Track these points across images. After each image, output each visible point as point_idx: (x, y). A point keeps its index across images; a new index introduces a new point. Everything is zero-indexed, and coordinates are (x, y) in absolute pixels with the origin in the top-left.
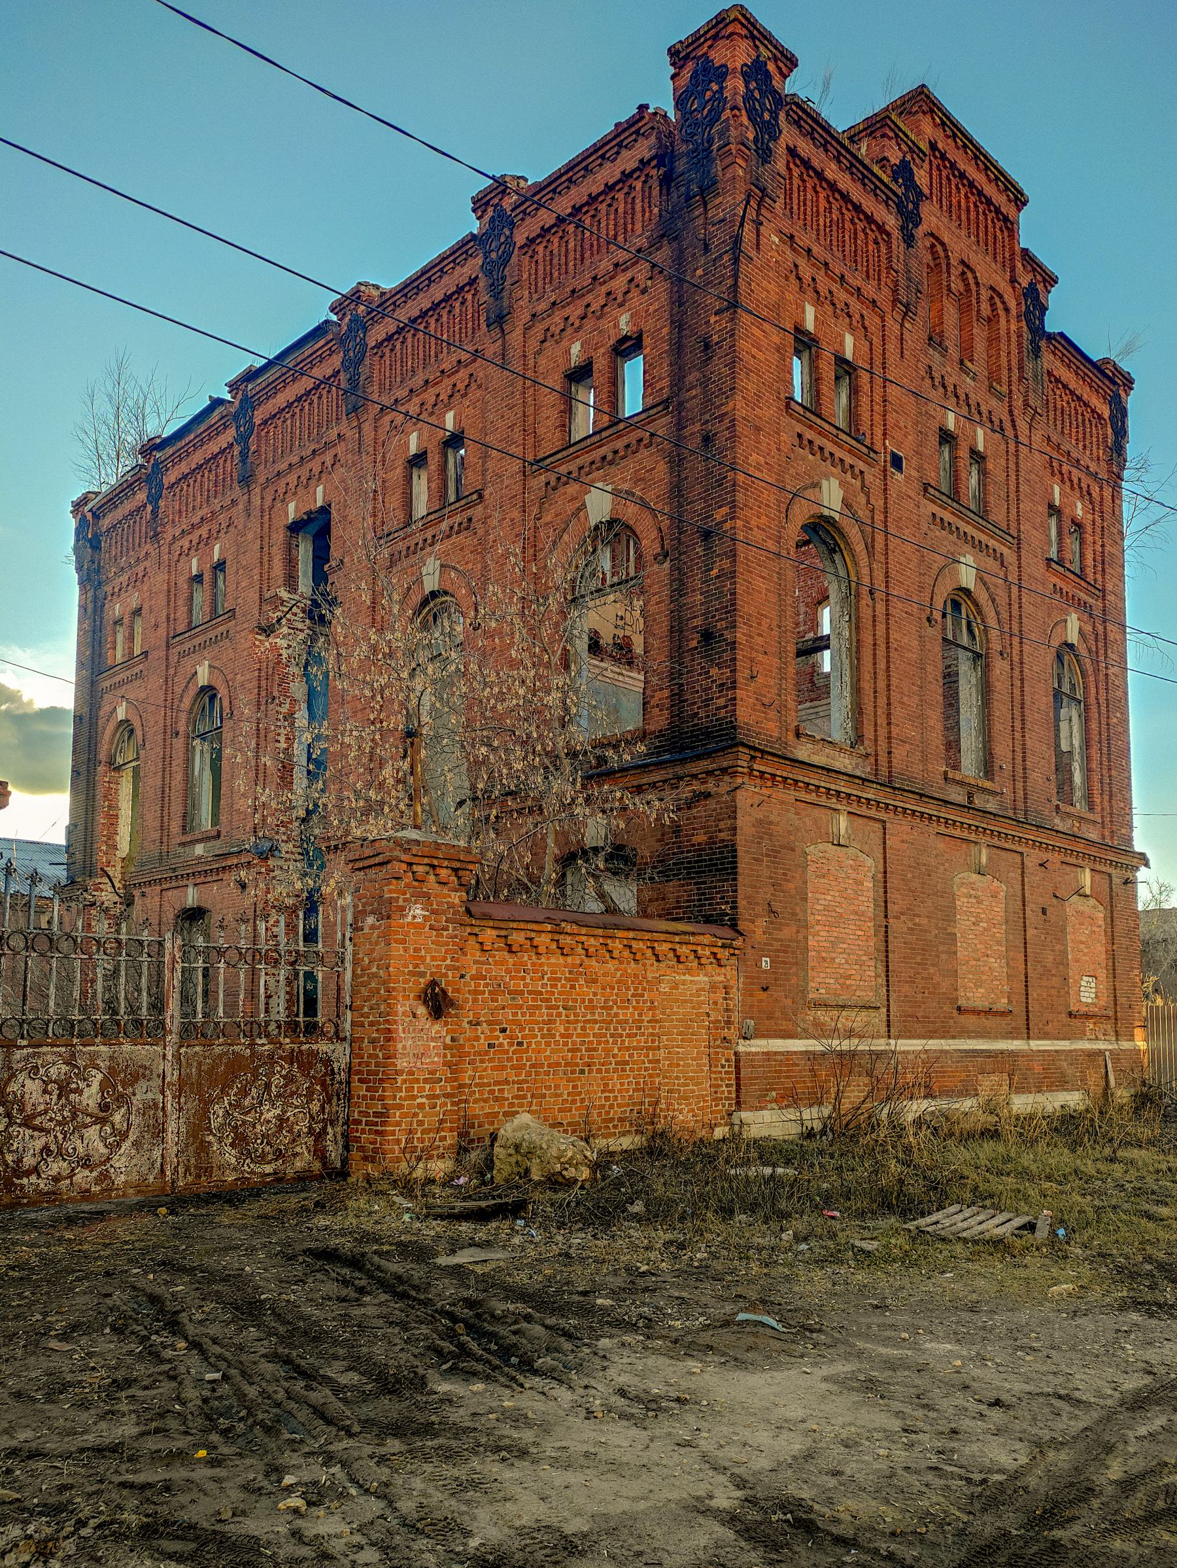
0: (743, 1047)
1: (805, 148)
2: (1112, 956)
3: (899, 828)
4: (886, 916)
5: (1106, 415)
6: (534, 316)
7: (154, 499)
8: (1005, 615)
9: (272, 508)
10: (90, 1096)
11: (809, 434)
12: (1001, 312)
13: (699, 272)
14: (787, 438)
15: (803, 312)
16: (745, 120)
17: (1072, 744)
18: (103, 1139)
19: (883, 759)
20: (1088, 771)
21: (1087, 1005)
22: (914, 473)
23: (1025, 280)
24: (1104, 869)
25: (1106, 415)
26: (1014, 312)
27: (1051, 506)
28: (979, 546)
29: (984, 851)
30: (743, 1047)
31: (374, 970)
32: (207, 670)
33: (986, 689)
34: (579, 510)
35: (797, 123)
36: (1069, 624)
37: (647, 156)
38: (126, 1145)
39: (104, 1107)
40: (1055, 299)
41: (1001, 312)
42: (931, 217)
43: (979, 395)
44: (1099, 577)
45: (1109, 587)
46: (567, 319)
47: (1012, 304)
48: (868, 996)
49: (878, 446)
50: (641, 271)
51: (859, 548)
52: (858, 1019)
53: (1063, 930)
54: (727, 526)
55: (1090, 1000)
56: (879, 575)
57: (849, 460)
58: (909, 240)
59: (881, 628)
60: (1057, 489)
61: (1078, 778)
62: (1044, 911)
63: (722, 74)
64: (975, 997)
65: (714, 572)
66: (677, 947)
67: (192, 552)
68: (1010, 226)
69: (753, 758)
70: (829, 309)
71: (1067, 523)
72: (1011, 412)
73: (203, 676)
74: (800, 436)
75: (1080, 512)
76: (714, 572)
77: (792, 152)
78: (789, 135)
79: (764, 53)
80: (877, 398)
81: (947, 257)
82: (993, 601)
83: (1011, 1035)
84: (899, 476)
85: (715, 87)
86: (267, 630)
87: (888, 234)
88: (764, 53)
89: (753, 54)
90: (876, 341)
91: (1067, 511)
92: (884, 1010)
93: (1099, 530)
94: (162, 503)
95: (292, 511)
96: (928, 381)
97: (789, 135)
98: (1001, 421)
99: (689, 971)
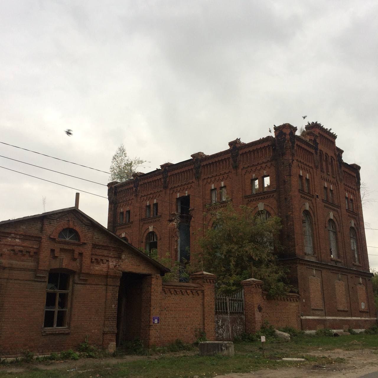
0: (302, 318)
1: (299, 143)
2: (367, 297)
3: (324, 271)
4: (323, 291)
5: (355, 176)
6: (244, 167)
7: (136, 187)
8: (339, 223)
9: (172, 194)
10: (220, 323)
11: (303, 195)
12: (333, 160)
13: (282, 168)
14: (299, 197)
15: (300, 172)
16: (290, 142)
17: (354, 248)
18: (222, 331)
19: (320, 257)
20: (358, 255)
21: (363, 309)
22: (321, 198)
23: (337, 153)
24: (364, 277)
25: (355, 176)
26: (336, 160)
27: (346, 197)
28: (334, 210)
29: (340, 275)
30: (302, 318)
31: (250, 303)
32: (152, 228)
33: (337, 239)
34: (256, 207)
35: (298, 140)
36: (352, 223)
37: (270, 144)
38: (225, 332)
39: (222, 326)
40: (343, 155)
41: (333, 160)
42: (320, 147)
43: (331, 178)
44: (357, 211)
45: (359, 213)
46: (251, 169)
47: (335, 158)
48: (322, 308)
49: (314, 195)
50: (269, 164)
51: (312, 215)
52: (319, 313)
53: (357, 292)
54: (291, 215)
55: (364, 308)
56: (316, 219)
57: (309, 198)
58: (316, 153)
59: (317, 230)
60: (347, 194)
61: (356, 256)
62: (353, 288)
63: (285, 134)
64: (341, 308)
65: (289, 224)
66: (192, 290)
67: (147, 200)
68: (334, 143)
69: (300, 260)
70: (304, 170)
71: (349, 200)
72: (337, 180)
73: (151, 229)
74: (301, 196)
75: (352, 197)
76: (289, 224)
77: (297, 145)
78: (297, 142)
79: (292, 130)
80: (313, 185)
81: (323, 153)
82: (337, 220)
83: (348, 316)
84: (318, 199)
85: (284, 136)
86: (171, 221)
87: (313, 154)
88: (292, 130)
89: (290, 130)
90: (312, 173)
91: (349, 198)
92: (324, 310)
93: (356, 200)
94: (139, 188)
95: (178, 195)
96: (321, 179)
97: (297, 142)
98: (335, 182)
99: (292, 303)
